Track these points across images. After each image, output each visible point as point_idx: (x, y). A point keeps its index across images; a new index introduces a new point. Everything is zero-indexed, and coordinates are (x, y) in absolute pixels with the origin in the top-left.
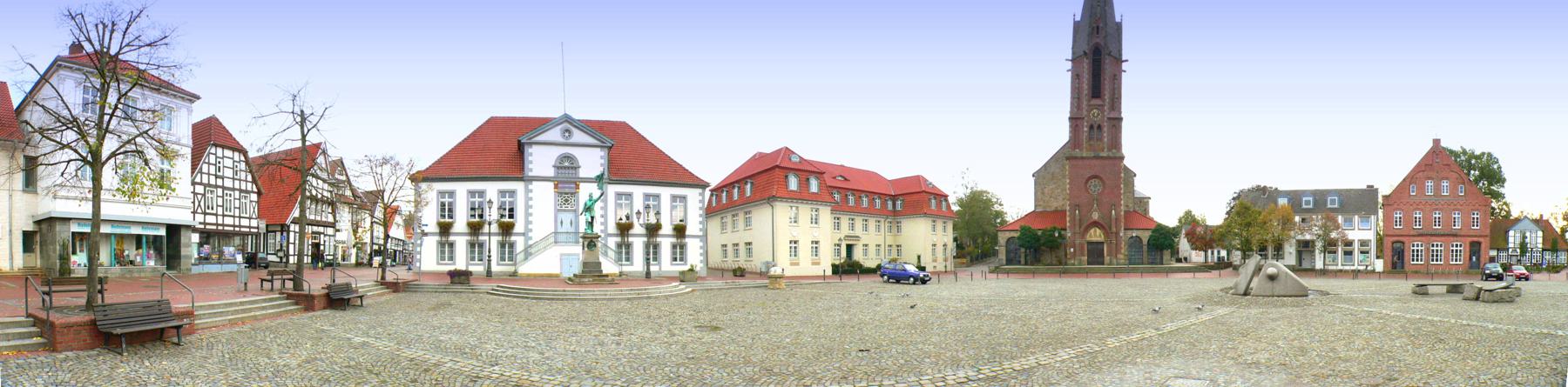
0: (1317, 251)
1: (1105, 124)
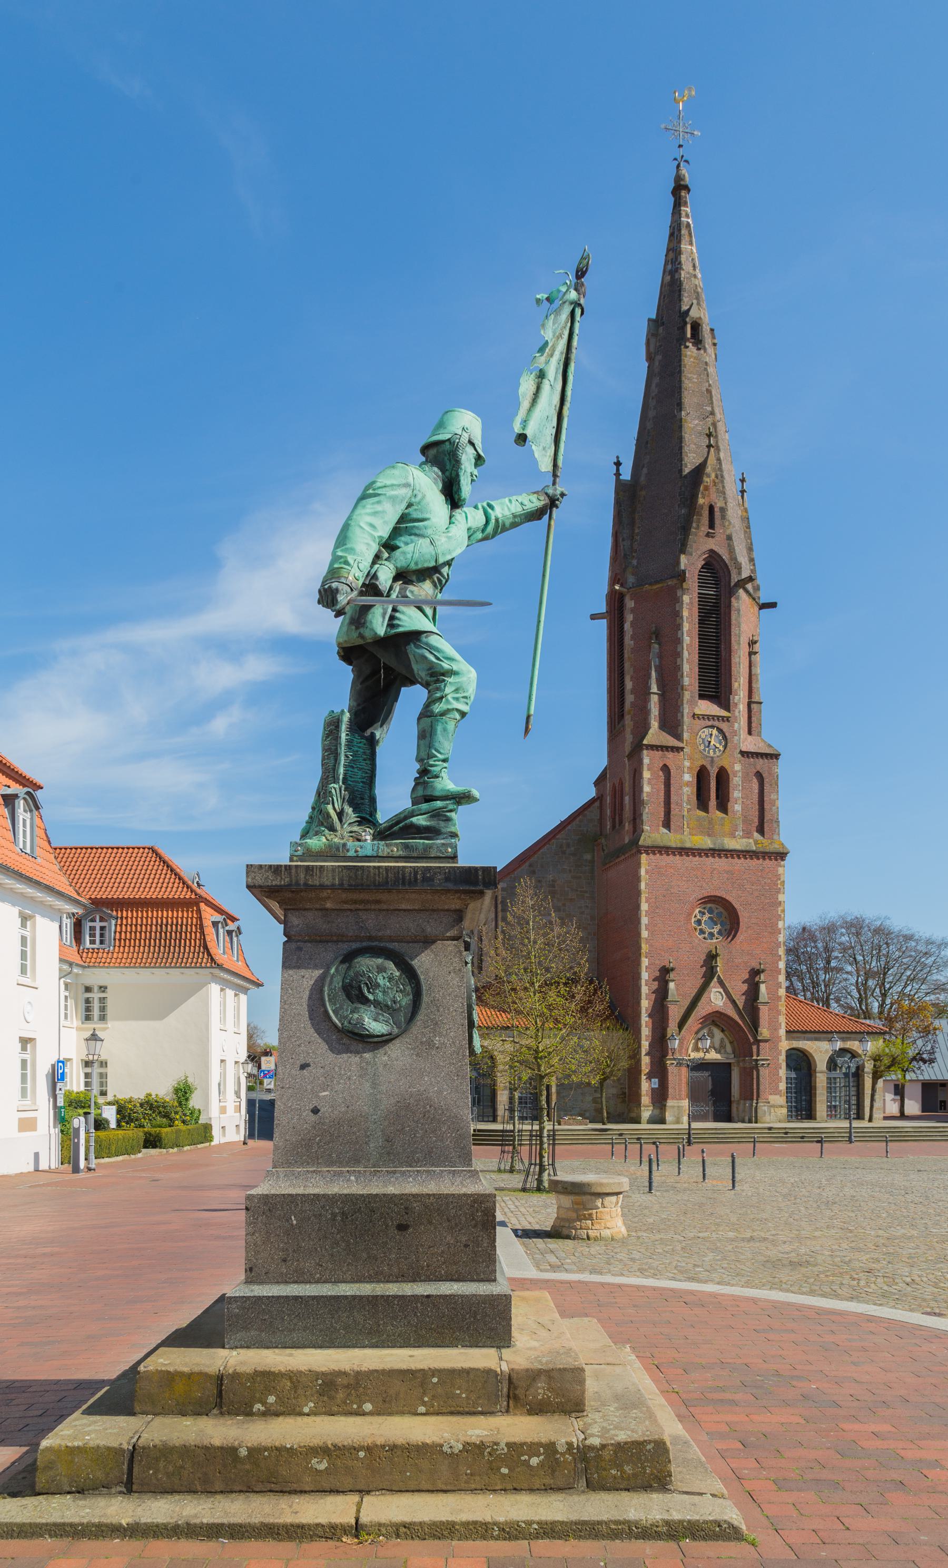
0: (644, 1077)
1: (737, 767)
